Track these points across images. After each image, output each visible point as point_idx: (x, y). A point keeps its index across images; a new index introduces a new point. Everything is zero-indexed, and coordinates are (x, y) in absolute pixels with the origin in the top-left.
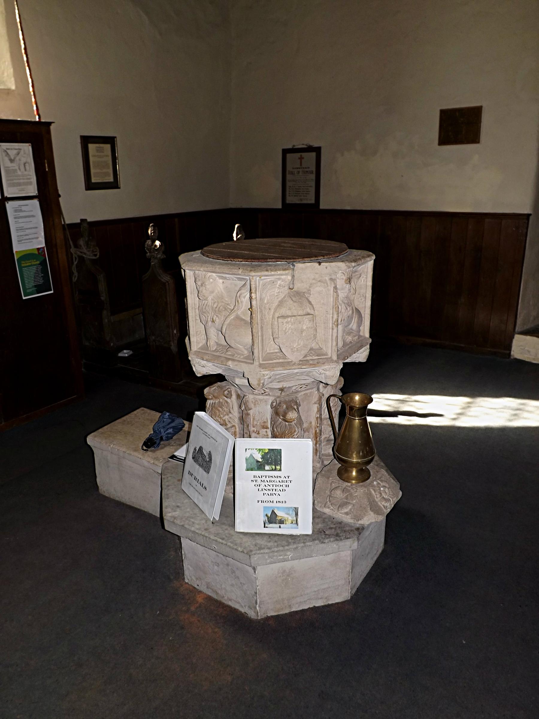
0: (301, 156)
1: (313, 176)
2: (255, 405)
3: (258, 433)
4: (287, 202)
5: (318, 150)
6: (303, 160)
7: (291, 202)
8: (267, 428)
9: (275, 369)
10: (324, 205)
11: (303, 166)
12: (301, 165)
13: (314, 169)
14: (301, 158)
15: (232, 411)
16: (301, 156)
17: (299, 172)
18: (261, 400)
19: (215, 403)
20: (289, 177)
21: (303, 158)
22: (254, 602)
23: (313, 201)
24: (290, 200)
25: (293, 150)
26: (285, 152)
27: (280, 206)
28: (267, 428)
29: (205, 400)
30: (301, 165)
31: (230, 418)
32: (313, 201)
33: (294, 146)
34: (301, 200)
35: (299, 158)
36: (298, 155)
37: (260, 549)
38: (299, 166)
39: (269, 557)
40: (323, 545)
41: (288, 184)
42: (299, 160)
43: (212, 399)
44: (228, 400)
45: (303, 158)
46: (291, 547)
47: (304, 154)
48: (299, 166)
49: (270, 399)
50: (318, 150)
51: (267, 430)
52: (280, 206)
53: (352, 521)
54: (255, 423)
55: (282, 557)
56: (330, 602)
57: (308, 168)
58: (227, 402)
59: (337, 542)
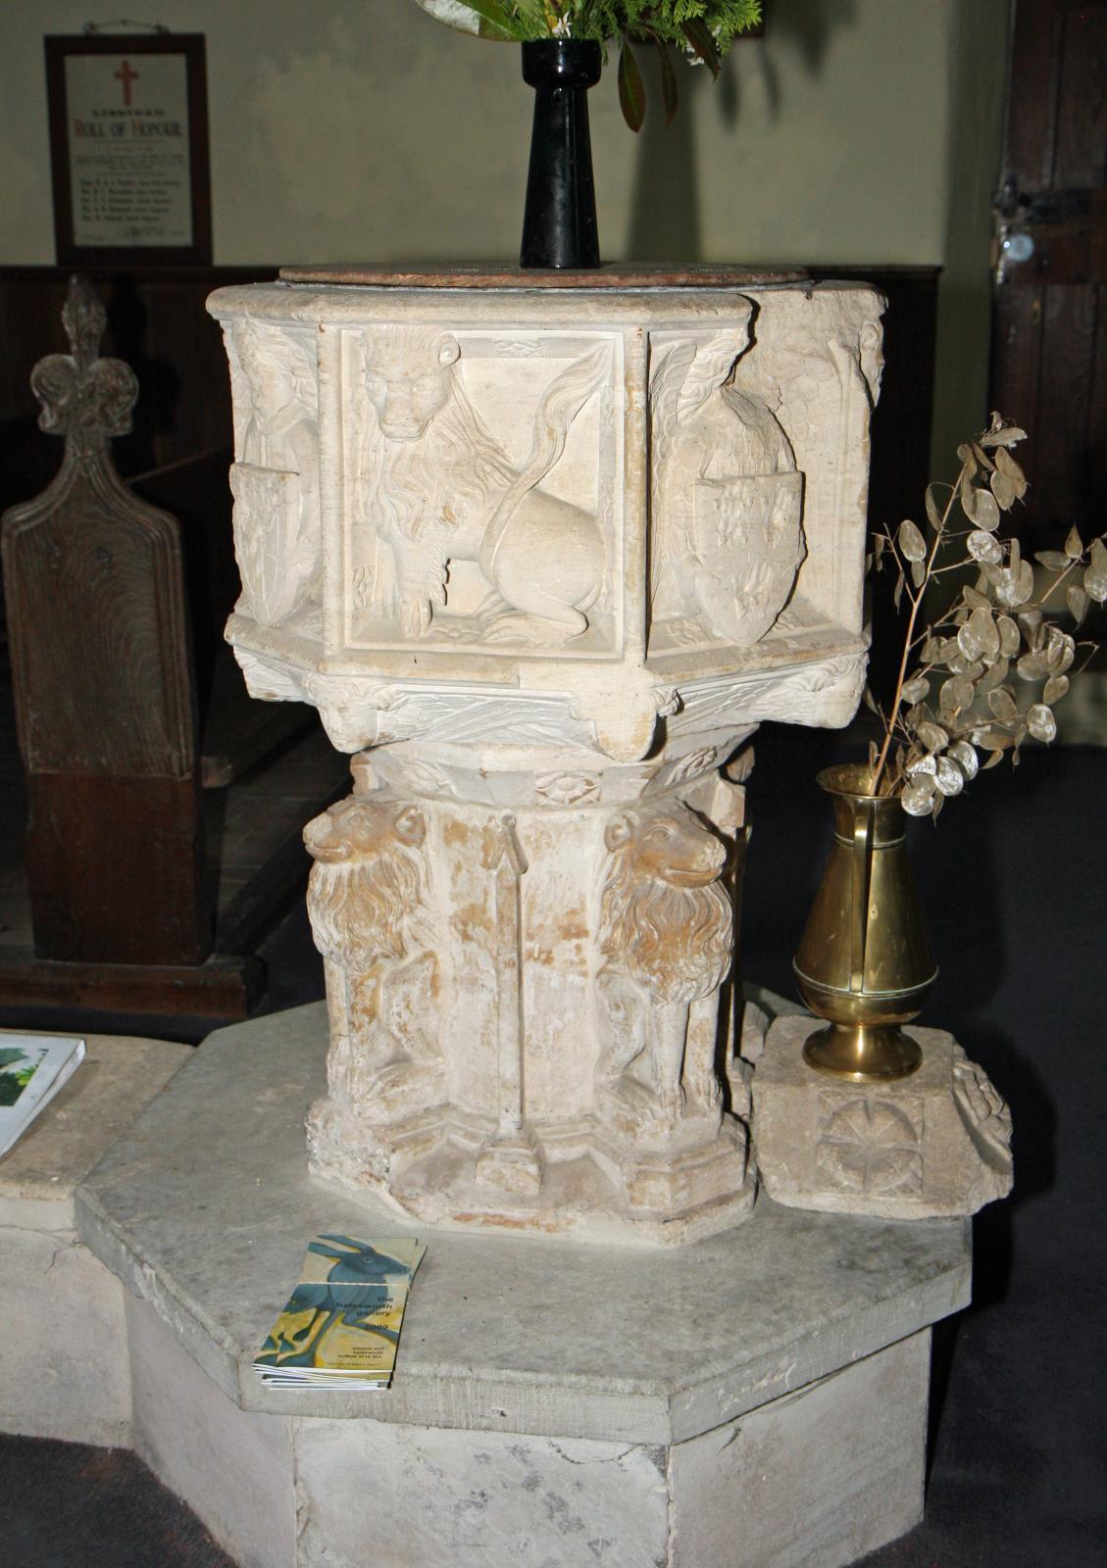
0: (126, 65)
1: (181, 146)
2: (537, 849)
3: (548, 961)
4: (79, 240)
5: (192, 48)
6: (134, 84)
7: (91, 242)
8: (581, 933)
9: (698, 674)
11: (135, 106)
12: (128, 100)
13: (181, 116)
14: (127, 75)
15: (424, 894)
16: (126, 65)
17: (121, 129)
19: (363, 869)
20: (78, 146)
21: (135, 76)
23: (185, 239)
24: (90, 232)
25: (93, 44)
27: (44, 254)
28: (581, 933)
29: (308, 861)
30: (128, 100)
31: (420, 923)
32: (185, 239)
33: (92, 26)
34: (135, 232)
35: (118, 75)
36: (115, 62)
37: (694, 1364)
38: (118, 104)
40: (881, 1306)
41: (78, 174)
42: (119, 84)
43: (349, 856)
45: (135, 76)
46: (788, 1336)
47: (136, 62)
48: (118, 104)
49: (597, 822)
50: (192, 48)
51: (582, 941)
52: (44, 254)
53: (930, 1211)
54: (536, 920)
55: (764, 1383)
56: (874, 1545)
57: (159, 113)
58: (408, 862)
59: (917, 1289)
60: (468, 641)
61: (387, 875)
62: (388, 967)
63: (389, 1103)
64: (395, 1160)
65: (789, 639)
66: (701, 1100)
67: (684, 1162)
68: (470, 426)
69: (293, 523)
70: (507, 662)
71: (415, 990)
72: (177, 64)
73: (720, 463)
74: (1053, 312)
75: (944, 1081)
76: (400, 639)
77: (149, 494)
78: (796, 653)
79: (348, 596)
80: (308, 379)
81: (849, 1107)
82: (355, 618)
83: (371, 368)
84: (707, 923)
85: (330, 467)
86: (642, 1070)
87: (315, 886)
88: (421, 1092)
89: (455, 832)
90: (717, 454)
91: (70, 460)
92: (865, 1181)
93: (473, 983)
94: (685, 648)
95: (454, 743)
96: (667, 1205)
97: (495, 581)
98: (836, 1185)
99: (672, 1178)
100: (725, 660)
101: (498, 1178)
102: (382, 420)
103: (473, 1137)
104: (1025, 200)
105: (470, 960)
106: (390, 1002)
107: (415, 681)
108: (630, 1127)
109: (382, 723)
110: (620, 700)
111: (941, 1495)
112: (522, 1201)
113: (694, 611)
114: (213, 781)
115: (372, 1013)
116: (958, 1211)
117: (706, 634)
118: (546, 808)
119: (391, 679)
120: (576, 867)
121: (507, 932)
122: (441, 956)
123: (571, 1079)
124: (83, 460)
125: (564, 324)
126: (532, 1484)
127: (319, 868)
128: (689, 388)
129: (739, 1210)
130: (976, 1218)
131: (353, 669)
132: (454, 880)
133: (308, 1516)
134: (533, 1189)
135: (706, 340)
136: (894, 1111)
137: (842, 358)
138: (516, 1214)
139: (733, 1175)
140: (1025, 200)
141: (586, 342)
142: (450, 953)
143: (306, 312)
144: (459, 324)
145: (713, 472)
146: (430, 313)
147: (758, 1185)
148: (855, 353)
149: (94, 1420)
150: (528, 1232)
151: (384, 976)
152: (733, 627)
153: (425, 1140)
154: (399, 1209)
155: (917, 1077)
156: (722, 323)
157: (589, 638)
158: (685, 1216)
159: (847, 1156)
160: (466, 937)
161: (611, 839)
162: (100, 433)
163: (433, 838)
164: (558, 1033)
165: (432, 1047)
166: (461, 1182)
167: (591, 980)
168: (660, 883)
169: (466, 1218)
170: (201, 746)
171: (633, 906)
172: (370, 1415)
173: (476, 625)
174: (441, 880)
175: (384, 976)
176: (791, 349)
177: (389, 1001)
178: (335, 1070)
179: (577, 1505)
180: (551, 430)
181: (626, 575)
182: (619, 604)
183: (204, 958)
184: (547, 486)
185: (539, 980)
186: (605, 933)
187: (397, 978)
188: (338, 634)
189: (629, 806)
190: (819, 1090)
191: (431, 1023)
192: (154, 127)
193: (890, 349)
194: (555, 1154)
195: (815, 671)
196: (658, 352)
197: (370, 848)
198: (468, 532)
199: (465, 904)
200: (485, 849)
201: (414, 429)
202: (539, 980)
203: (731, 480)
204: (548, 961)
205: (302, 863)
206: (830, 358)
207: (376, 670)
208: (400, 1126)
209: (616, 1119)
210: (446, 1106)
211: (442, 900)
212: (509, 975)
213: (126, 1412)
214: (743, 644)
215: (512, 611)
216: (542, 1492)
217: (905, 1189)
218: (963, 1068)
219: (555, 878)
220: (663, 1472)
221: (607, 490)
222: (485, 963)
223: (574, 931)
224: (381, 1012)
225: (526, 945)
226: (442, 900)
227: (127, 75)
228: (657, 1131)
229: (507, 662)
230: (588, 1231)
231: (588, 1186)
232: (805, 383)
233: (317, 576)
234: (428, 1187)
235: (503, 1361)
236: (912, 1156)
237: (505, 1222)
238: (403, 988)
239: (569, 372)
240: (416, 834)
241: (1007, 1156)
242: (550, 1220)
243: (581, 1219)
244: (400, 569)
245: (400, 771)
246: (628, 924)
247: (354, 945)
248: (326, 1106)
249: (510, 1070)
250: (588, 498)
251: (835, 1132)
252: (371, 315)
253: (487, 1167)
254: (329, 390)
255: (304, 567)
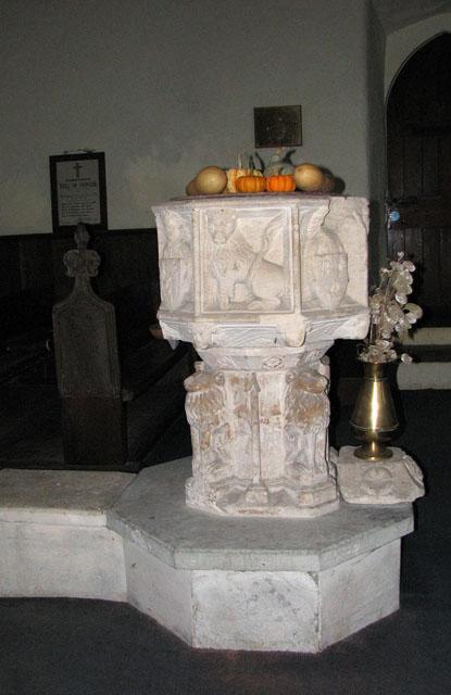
1: (97, 190)
3: (268, 423)
4: (61, 224)
5: (100, 157)
8: (279, 413)
10: (114, 224)
14: (78, 167)
17: (75, 185)
18: (271, 377)
20: (60, 191)
22: (314, 630)
24: (66, 220)
25: (66, 158)
26: (54, 160)
27: (48, 229)
28: (279, 413)
29: (186, 392)
32: (98, 222)
36: (73, 163)
38: (75, 177)
39: (338, 553)
41: (61, 201)
42: (75, 171)
43: (200, 389)
44: (221, 388)
47: (81, 162)
49: (283, 375)
50: (100, 157)
52: (48, 229)
53: (398, 501)
56: (384, 616)
58: (218, 390)
60: (245, 311)
61: (213, 395)
62: (213, 428)
63: (215, 475)
64: (218, 493)
65: (347, 309)
66: (321, 468)
67: (316, 489)
68: (241, 239)
69: (183, 273)
70: (256, 315)
71: (223, 435)
72: (96, 161)
73: (322, 249)
74: (408, 239)
75: (400, 460)
76: (220, 310)
77: (105, 298)
78: (349, 312)
79: (202, 296)
80: (187, 229)
81: (371, 469)
82: (205, 303)
83: (210, 220)
84: (322, 405)
85: (196, 254)
86: (301, 460)
87: (188, 401)
88: (226, 472)
89: (235, 380)
90: (320, 246)
91: (77, 284)
92: (377, 492)
93: (243, 432)
94: (312, 310)
95: (235, 347)
96: (312, 503)
97: (250, 288)
98: (367, 494)
99: (313, 494)
100: (326, 314)
101: (254, 497)
102: (214, 238)
103: (244, 486)
104: (395, 200)
105: (241, 425)
106: (215, 440)
107: (226, 323)
108: (298, 478)
109: (214, 338)
110: (293, 326)
111: (403, 601)
112: (263, 505)
113: (315, 298)
114: (127, 398)
115: (208, 444)
116: (408, 500)
117: (319, 306)
118: (266, 370)
119: (217, 323)
120: (276, 390)
121: (252, 413)
122: (231, 424)
123: (276, 464)
124: (82, 285)
125: (272, 205)
126: (273, 591)
127: (190, 394)
128: (311, 225)
129: (335, 506)
130: (414, 503)
131: (205, 320)
132: (235, 397)
133: (197, 608)
134: (266, 501)
135: (315, 210)
136: (386, 469)
137: (357, 217)
138: (260, 509)
139: (333, 494)
140: (395, 200)
141: (279, 211)
142: (234, 422)
143: (188, 205)
144: (239, 206)
145: (319, 252)
146: (229, 203)
147: (341, 498)
148: (361, 216)
149: (117, 592)
150: (265, 516)
151: (212, 431)
152: (328, 302)
153: (227, 488)
154: (220, 511)
155: (391, 459)
156: (321, 205)
157: (283, 308)
158: (318, 506)
159: (371, 485)
160: (239, 417)
161: (288, 380)
162: (87, 276)
163: (227, 383)
164: (272, 448)
165: (228, 456)
166: (241, 500)
167: (282, 431)
168: (306, 393)
169: (244, 512)
170: (123, 385)
171: (297, 401)
172: (218, 568)
173: (245, 305)
174: (230, 397)
175: (212, 431)
176: (341, 215)
177: (214, 440)
178: (195, 466)
179: (288, 597)
180: (266, 238)
181: (294, 284)
182: (292, 294)
183: (125, 462)
184: (267, 257)
185: (265, 429)
186: (287, 412)
187: (216, 432)
188: (199, 309)
189: (292, 369)
190: (360, 465)
191: (228, 447)
192: (87, 184)
193: (371, 216)
194: (272, 490)
195: (354, 319)
196: (301, 213)
197: (206, 387)
198: (241, 274)
199: (239, 405)
200: (246, 385)
201: (224, 240)
202: (265, 429)
203: (325, 255)
204: (268, 423)
205: (184, 393)
206: (353, 217)
207: (212, 320)
208: (218, 483)
209: (293, 476)
210: (233, 477)
211: (231, 404)
212: (255, 427)
213: (125, 590)
214: (331, 309)
215: (258, 299)
216: (276, 593)
217: (390, 494)
218: (405, 457)
219: (270, 394)
220: (317, 583)
221: (286, 258)
222: (247, 425)
223: (276, 412)
224: (211, 444)
225: (261, 418)
226: (231, 404)
227: (78, 167)
228: (307, 479)
229: (256, 315)
230: (284, 513)
231: (284, 499)
232: (346, 226)
233: (190, 294)
234: (230, 503)
235: (263, 548)
236: (394, 483)
237: (256, 512)
238: (219, 435)
239: (273, 221)
240: (222, 382)
241: (422, 484)
242: (272, 510)
243: (283, 509)
244: (227, 284)
245: (215, 360)
246: (294, 409)
247: (202, 420)
248: (192, 479)
249: (256, 461)
250: (280, 262)
251: (367, 478)
252: (211, 204)
253: (250, 494)
254: (196, 229)
255: (185, 289)
